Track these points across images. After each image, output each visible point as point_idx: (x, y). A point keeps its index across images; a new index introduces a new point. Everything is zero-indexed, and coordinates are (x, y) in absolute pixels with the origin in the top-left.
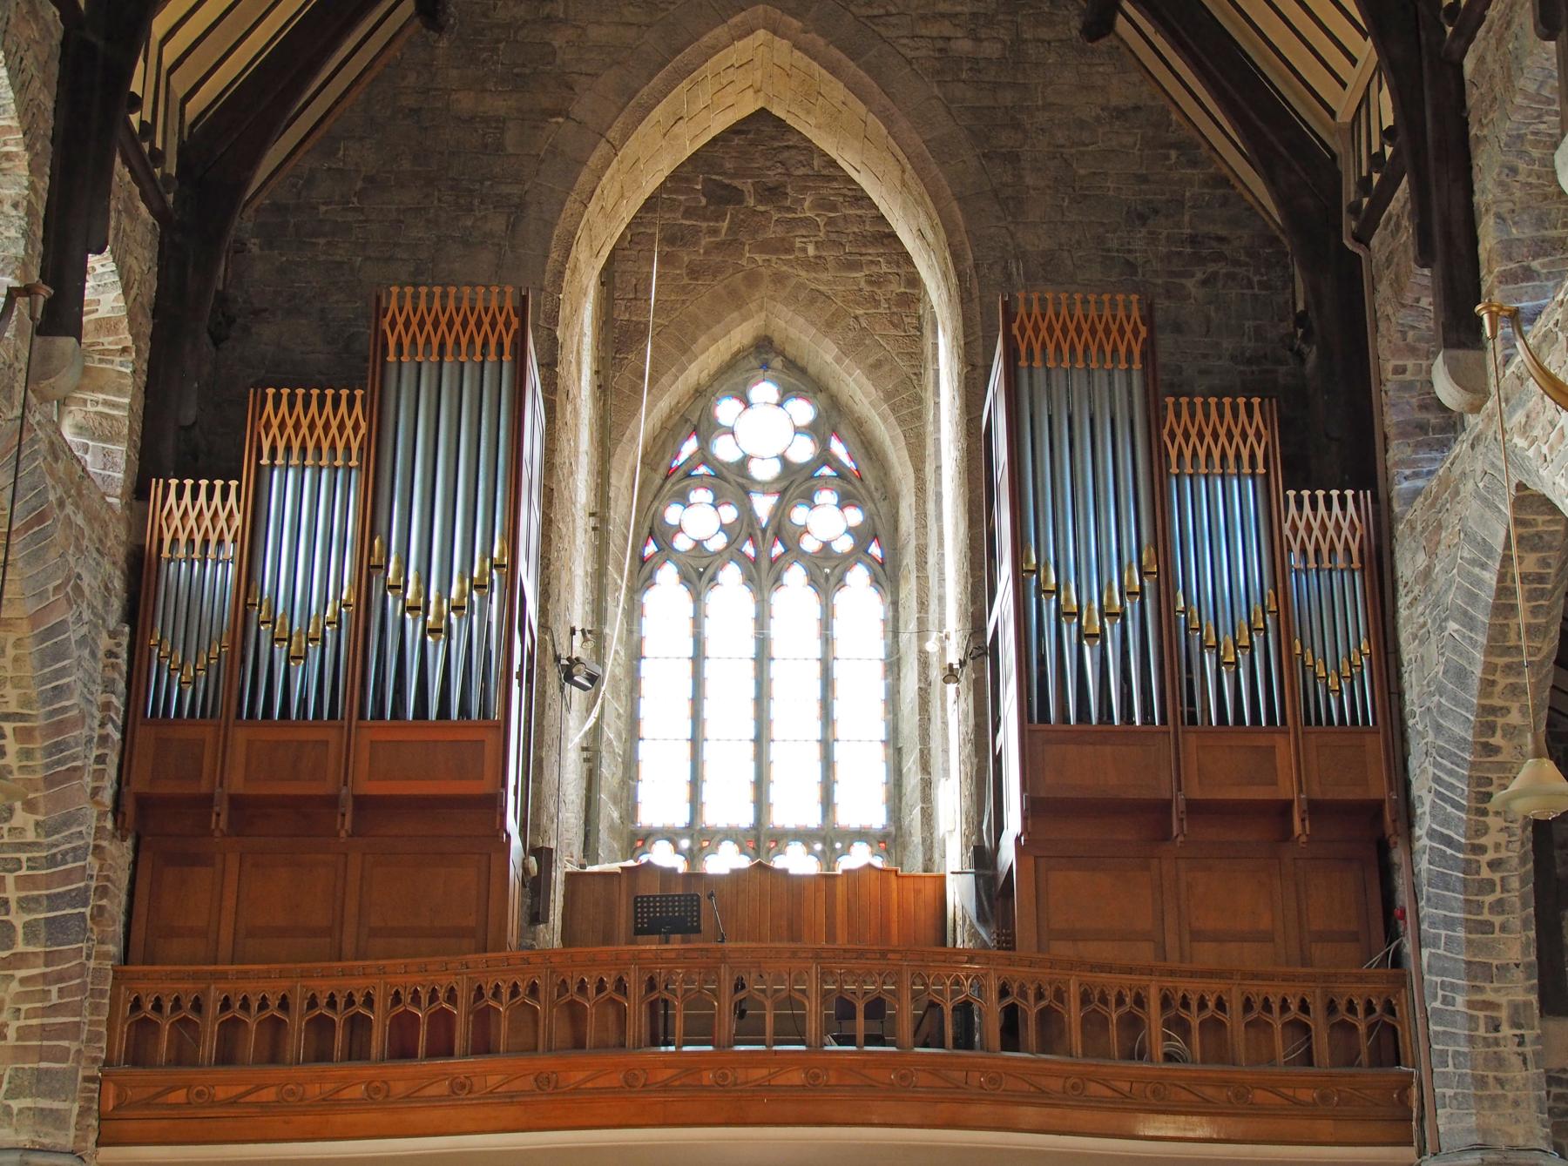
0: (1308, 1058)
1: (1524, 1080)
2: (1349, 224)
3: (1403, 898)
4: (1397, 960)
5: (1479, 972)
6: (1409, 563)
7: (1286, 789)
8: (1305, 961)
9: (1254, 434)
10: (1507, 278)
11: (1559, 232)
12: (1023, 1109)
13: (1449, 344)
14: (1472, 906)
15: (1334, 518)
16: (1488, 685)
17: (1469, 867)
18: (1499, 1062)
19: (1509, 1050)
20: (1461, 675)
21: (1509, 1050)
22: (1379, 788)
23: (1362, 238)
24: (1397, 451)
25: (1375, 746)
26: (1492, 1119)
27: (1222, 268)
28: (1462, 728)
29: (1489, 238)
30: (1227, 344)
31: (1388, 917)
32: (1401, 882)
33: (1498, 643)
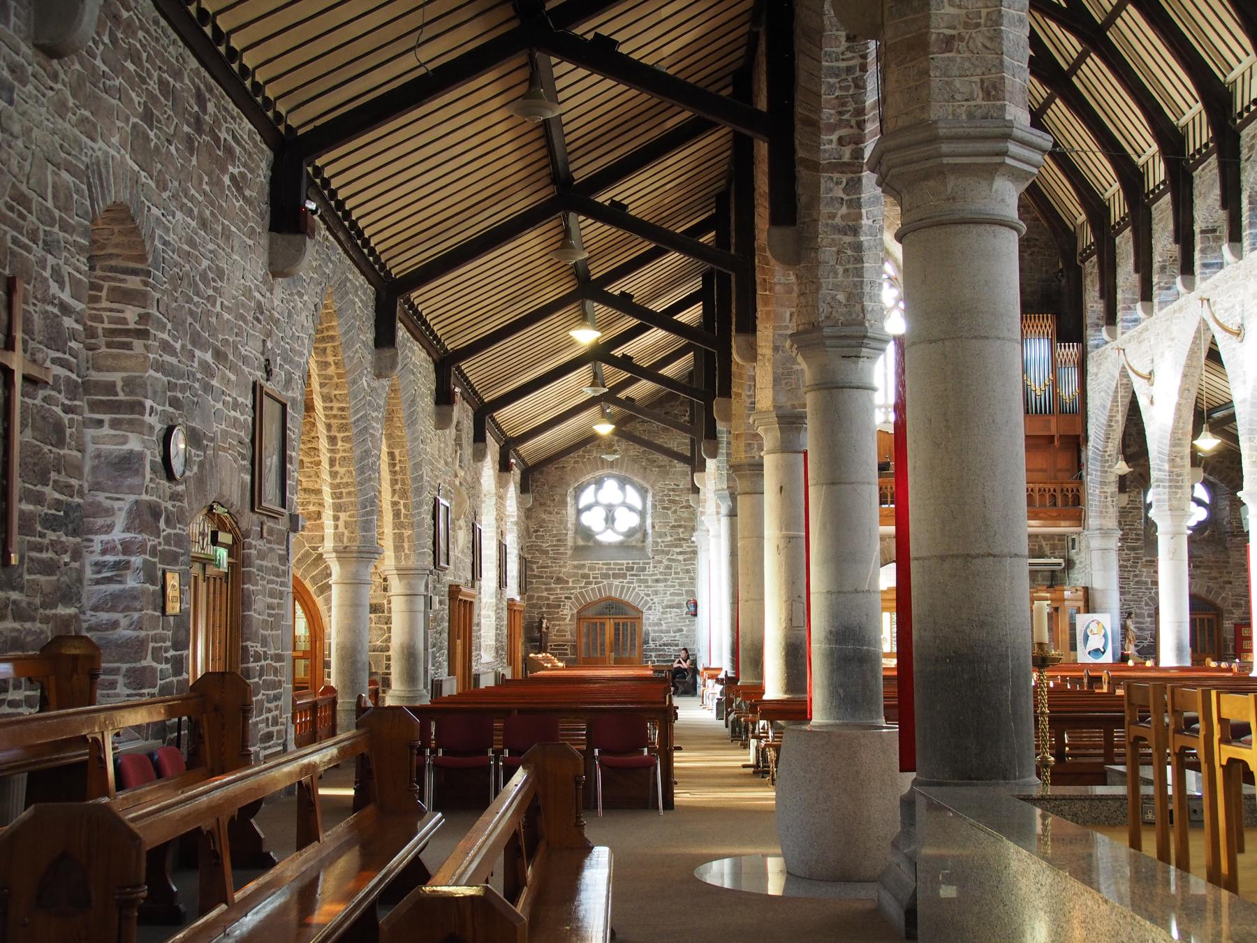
0: (1055, 505)
1: (1113, 512)
2: (1079, 258)
3: (1083, 460)
4: (1081, 477)
5: (1103, 483)
6: (1091, 368)
7: (1053, 431)
8: (1056, 478)
9: (1047, 324)
10: (1124, 309)
11: (1078, 933)
12: (417, 347)
13: (1107, 324)
14: (1103, 466)
15: (1070, 351)
16: (1111, 410)
17: (1102, 456)
18: (1107, 507)
19: (1109, 504)
20: (1104, 407)
21: (1109, 504)
22: (1079, 431)
23: (1083, 262)
24: (1089, 332)
25: (1079, 419)
26: (1103, 522)
27: (1036, 249)
28: (1103, 419)
29: (1119, 296)
30: (1037, 276)
31: (1078, 465)
32: (1083, 456)
33: (1115, 400)
